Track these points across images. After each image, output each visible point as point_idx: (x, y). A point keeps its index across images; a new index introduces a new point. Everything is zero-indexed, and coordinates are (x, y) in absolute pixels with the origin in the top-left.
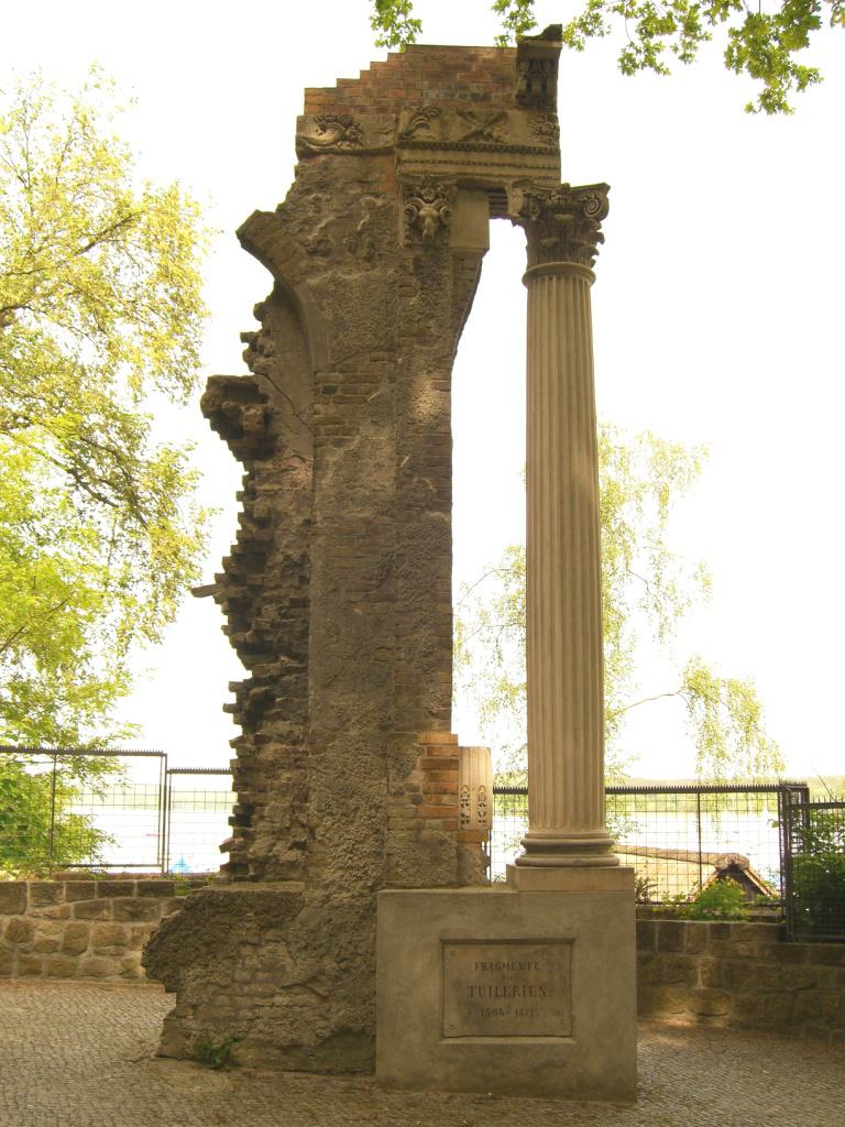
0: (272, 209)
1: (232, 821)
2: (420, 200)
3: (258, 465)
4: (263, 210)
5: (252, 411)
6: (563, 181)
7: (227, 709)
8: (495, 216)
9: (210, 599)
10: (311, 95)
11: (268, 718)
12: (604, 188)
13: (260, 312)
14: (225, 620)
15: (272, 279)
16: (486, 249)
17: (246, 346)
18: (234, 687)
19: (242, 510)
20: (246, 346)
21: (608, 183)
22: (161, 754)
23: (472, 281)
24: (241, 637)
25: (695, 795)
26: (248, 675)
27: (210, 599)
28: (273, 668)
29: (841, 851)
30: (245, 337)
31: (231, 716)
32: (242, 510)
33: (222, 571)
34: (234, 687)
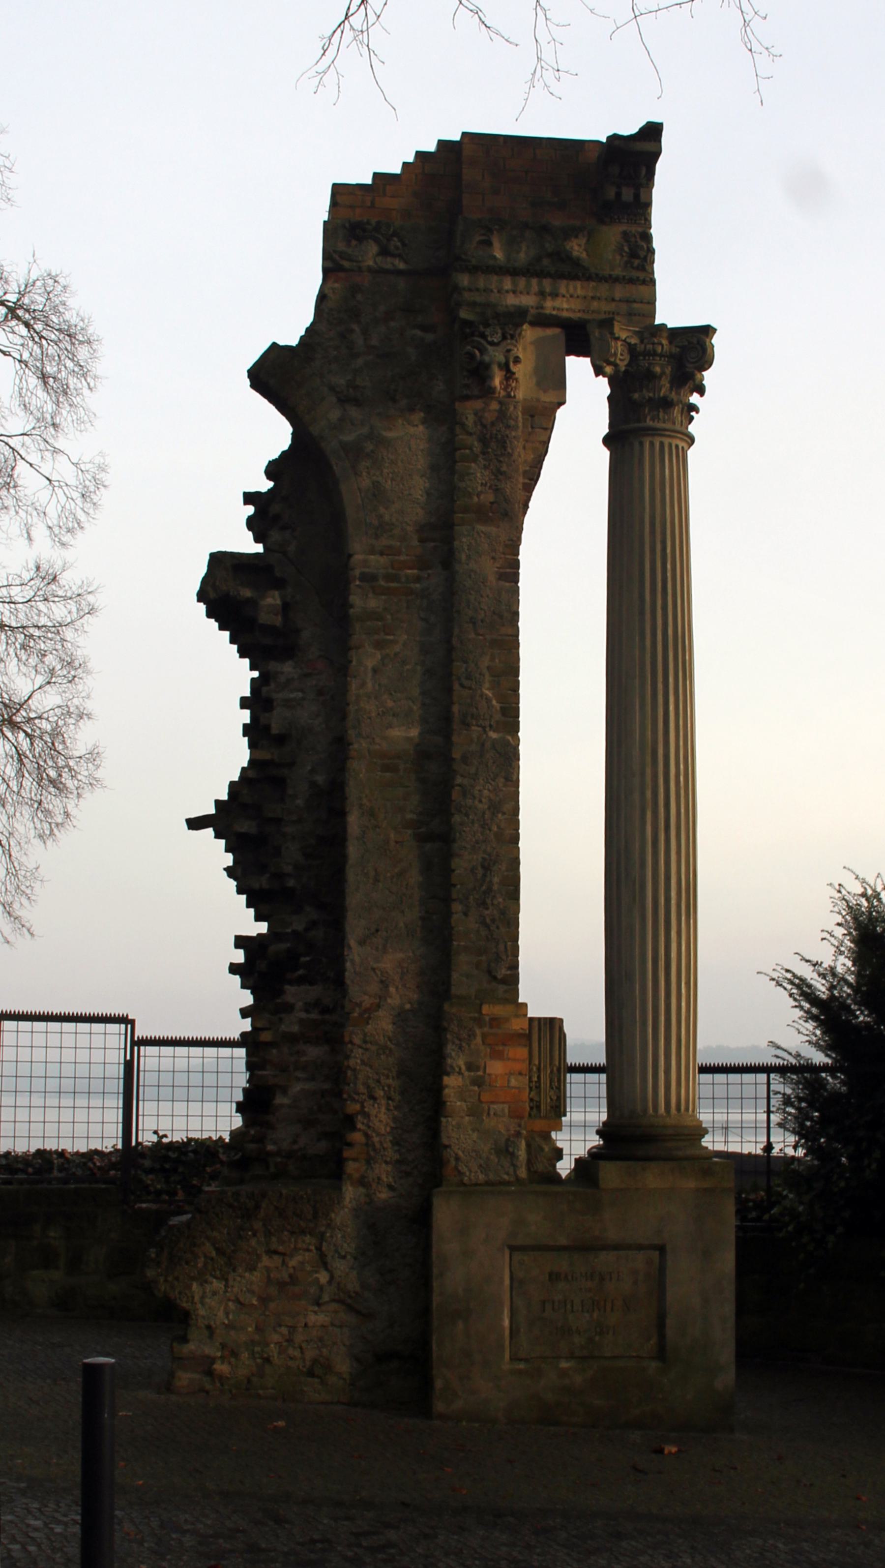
0: (293, 340)
1: (241, 1108)
2: (483, 341)
3: (273, 666)
4: (282, 343)
5: (269, 601)
6: (657, 322)
7: (234, 969)
8: (569, 355)
9: (210, 832)
10: (339, 192)
11: (291, 983)
12: (707, 331)
13: (273, 470)
14: (229, 859)
15: (289, 429)
16: (562, 403)
17: (250, 510)
18: (241, 942)
19: (248, 721)
20: (250, 510)
21: (714, 325)
22: (123, 1020)
23: (544, 442)
24: (262, 882)
25: (765, 1076)
26: (263, 927)
27: (210, 832)
28: (298, 924)
29: (825, 1094)
30: (249, 498)
31: (237, 979)
32: (248, 721)
33: (224, 797)
34: (241, 942)
